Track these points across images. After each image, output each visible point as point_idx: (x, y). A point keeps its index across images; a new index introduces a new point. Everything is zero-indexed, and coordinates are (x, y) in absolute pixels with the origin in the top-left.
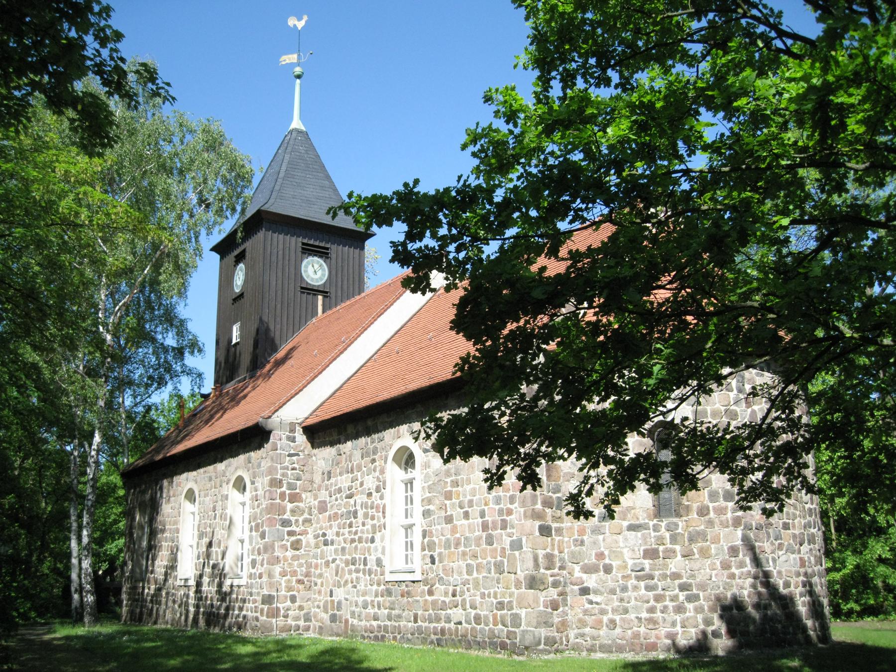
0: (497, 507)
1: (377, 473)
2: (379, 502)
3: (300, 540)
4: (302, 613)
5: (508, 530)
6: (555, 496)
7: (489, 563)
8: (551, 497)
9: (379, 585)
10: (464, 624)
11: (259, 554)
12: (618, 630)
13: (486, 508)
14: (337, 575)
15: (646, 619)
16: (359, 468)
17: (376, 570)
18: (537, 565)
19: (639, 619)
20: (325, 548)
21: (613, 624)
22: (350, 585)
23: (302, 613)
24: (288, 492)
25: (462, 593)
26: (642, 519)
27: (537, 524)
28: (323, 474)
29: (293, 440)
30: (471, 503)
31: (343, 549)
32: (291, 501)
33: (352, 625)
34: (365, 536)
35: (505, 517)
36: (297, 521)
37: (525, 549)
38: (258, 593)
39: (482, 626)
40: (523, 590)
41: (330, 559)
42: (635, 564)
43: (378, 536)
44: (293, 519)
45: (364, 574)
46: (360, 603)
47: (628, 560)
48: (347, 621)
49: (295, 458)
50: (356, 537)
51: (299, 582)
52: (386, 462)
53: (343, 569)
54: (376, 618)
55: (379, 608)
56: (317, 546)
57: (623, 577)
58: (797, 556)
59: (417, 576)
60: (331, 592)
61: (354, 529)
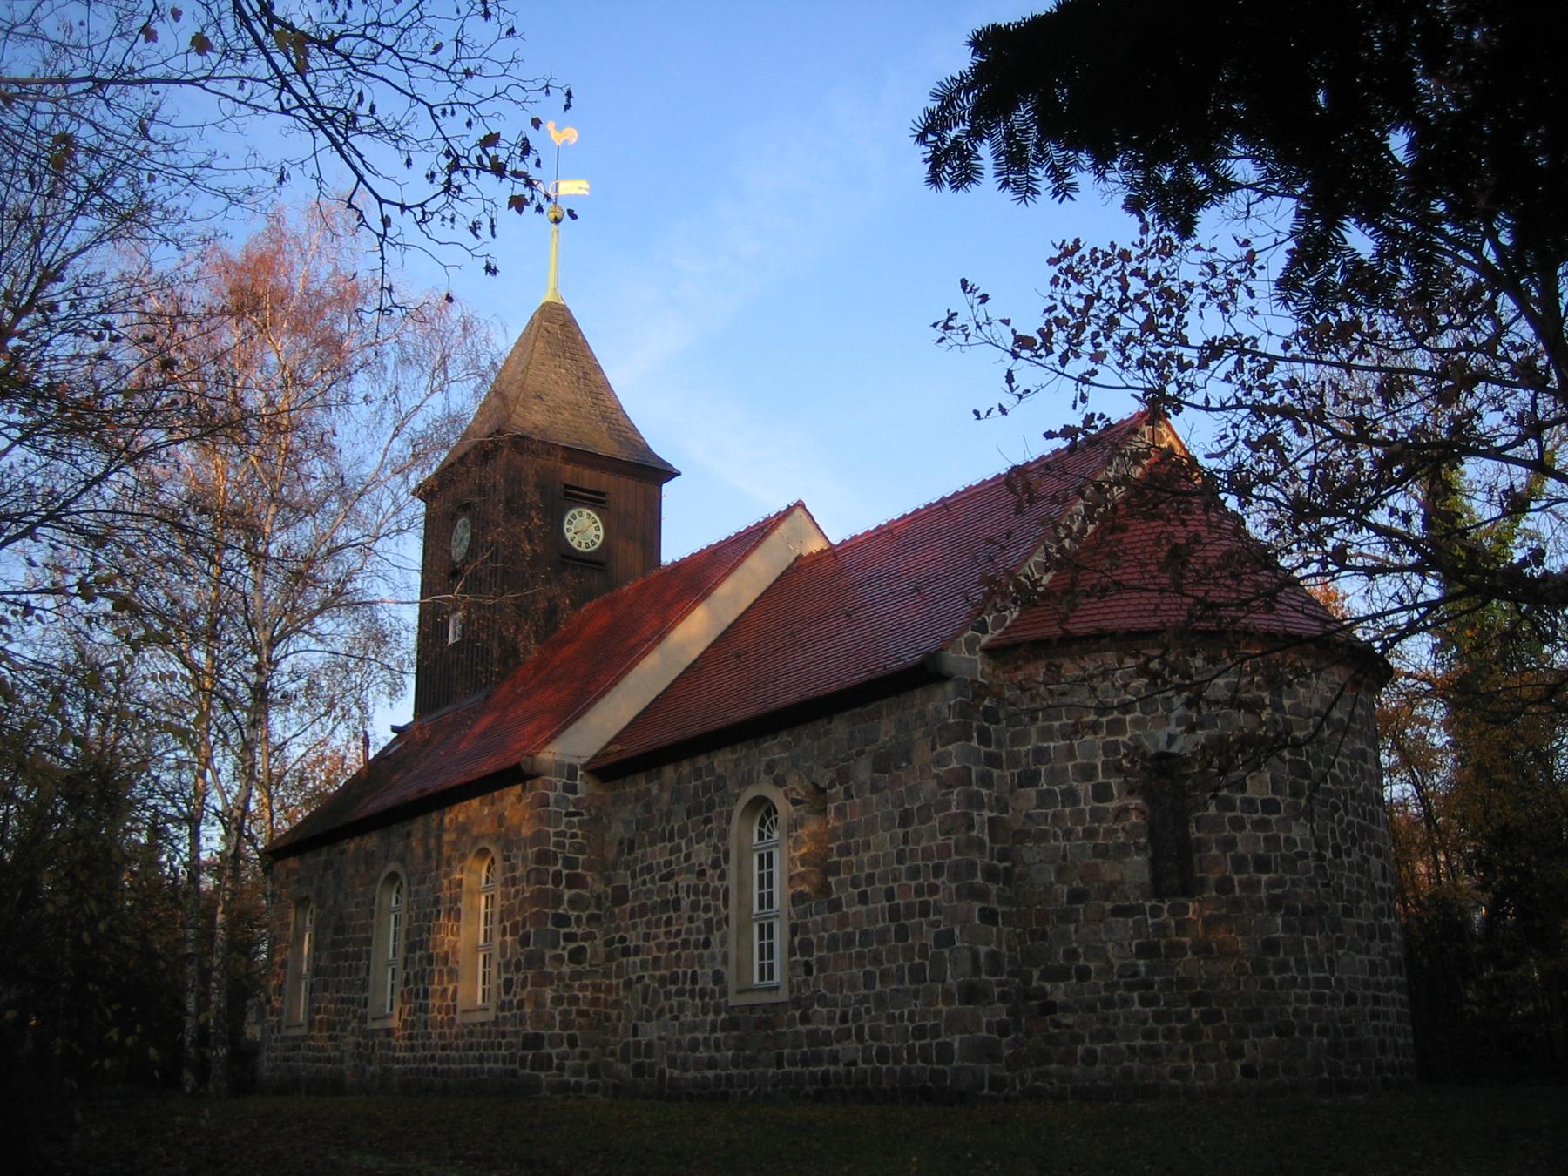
0: (913, 883)
1: (714, 840)
2: (717, 883)
3: (584, 948)
4: (586, 1063)
5: (932, 918)
6: (1001, 866)
7: (900, 968)
8: (996, 867)
9: (717, 1012)
10: (861, 1065)
11: (518, 969)
12: (1099, 1067)
13: (895, 886)
14: (645, 1002)
15: (1142, 1049)
16: (683, 832)
17: (713, 991)
18: (976, 969)
19: (1132, 1049)
20: (624, 960)
21: (1091, 1057)
22: (668, 1016)
23: (586, 1063)
24: (565, 872)
25: (857, 1016)
26: (1134, 899)
27: (977, 906)
28: (621, 843)
29: (572, 789)
30: (870, 879)
31: (656, 960)
32: (569, 887)
33: (671, 1078)
34: (693, 938)
35: (926, 898)
36: (579, 918)
37: (958, 944)
38: (516, 1034)
39: (891, 1065)
40: (957, 1006)
41: (634, 977)
42: (1124, 966)
43: (715, 938)
44: (573, 914)
45: (692, 997)
46: (685, 1043)
47: (1113, 960)
48: (662, 1072)
49: (575, 819)
50: (679, 941)
51: (581, 1013)
52: (728, 822)
53: (655, 991)
54: (712, 1064)
55: (718, 1048)
56: (610, 957)
57: (1106, 985)
58: (1365, 958)
59: (783, 995)
60: (635, 1028)
61: (674, 929)
